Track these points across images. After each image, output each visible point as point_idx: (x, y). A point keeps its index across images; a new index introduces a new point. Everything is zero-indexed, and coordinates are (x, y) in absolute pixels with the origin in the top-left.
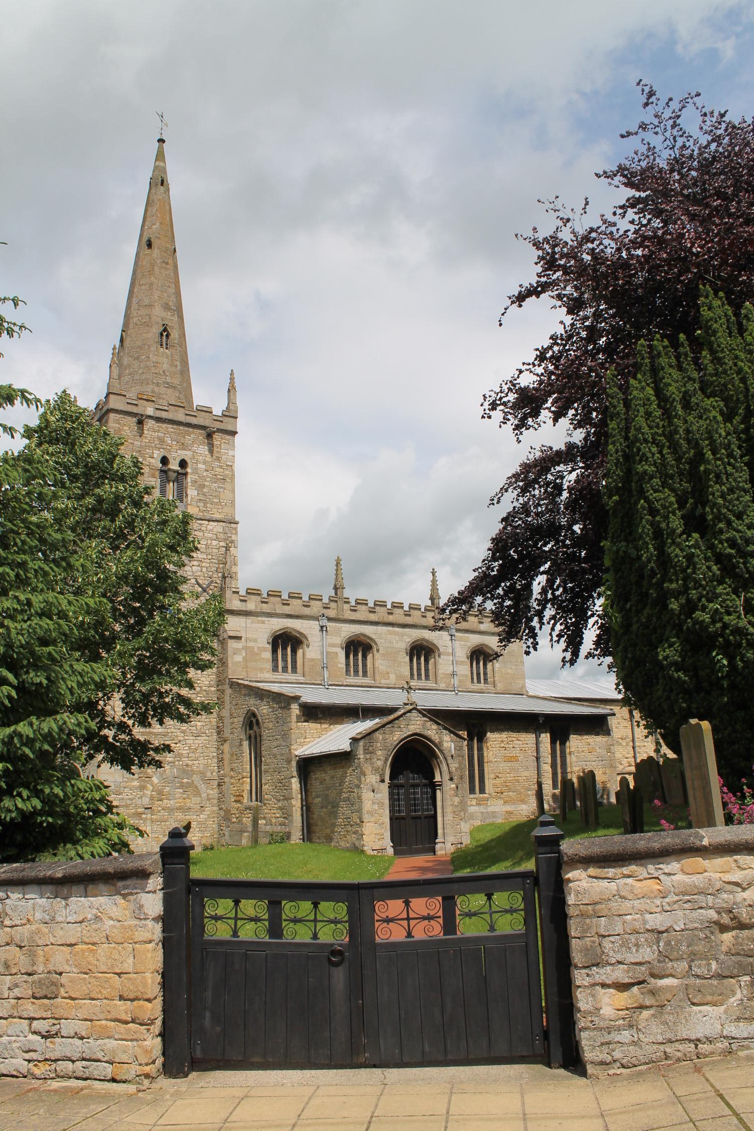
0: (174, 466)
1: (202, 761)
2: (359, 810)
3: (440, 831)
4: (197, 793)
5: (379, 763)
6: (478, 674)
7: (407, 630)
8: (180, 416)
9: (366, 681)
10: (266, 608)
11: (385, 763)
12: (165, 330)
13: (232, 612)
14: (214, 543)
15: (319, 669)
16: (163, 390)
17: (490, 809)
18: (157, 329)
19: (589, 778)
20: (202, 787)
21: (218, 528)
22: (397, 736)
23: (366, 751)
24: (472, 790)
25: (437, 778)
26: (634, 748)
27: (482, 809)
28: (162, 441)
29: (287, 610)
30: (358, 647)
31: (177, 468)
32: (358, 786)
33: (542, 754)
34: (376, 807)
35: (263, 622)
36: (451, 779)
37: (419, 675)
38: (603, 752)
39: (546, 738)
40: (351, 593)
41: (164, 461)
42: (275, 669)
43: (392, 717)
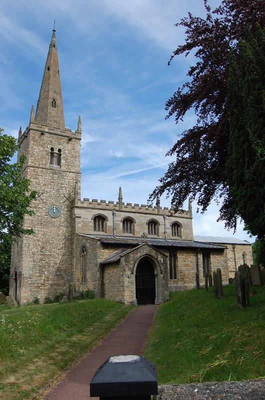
0: (56, 151)
1: (65, 266)
2: (123, 286)
4: (63, 278)
5: (132, 266)
7: (147, 215)
8: (59, 133)
10: (91, 206)
11: (134, 266)
12: (54, 100)
13: (78, 207)
14: (72, 181)
15: (112, 230)
16: (52, 123)
17: (179, 285)
18: (50, 100)
19: (218, 274)
20: (65, 276)
23: (126, 261)
24: (171, 278)
25: (156, 273)
26: (235, 262)
27: (175, 285)
28: (51, 141)
29: (100, 207)
31: (57, 152)
32: (122, 275)
35: (90, 212)
36: (161, 273)
37: (152, 232)
38: (223, 263)
39: (200, 257)
40: (125, 201)
41: (52, 149)
42: (95, 229)
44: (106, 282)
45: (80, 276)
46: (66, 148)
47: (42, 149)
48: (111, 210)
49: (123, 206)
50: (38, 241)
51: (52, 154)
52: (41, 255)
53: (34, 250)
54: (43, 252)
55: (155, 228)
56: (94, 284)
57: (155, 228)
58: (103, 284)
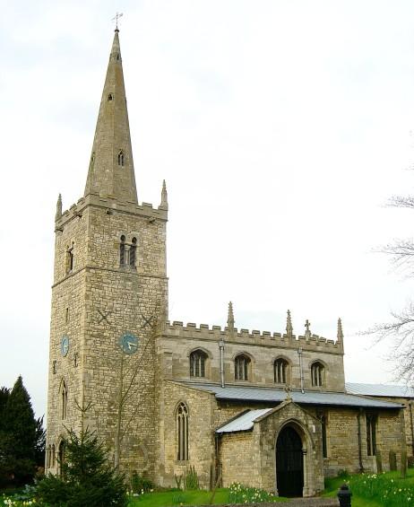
3: (305, 481)
6: (279, 378)
9: (247, 383)
21: (156, 282)
22: (281, 420)
25: (304, 448)
28: (121, 225)
29: (199, 336)
30: (243, 359)
31: (131, 243)
33: (362, 433)
34: (269, 465)
36: (314, 448)
39: (364, 421)
40: (239, 326)
41: (123, 238)
42: (191, 375)
43: (277, 408)
44: (225, 460)
45: (174, 452)
46: (144, 234)
47: (107, 237)
48: (218, 341)
49: (235, 334)
50: (105, 391)
51: (122, 246)
52: (109, 415)
53: (98, 407)
54: (111, 410)
55: (284, 371)
56: (203, 465)
57: (284, 371)
58: (218, 464)
